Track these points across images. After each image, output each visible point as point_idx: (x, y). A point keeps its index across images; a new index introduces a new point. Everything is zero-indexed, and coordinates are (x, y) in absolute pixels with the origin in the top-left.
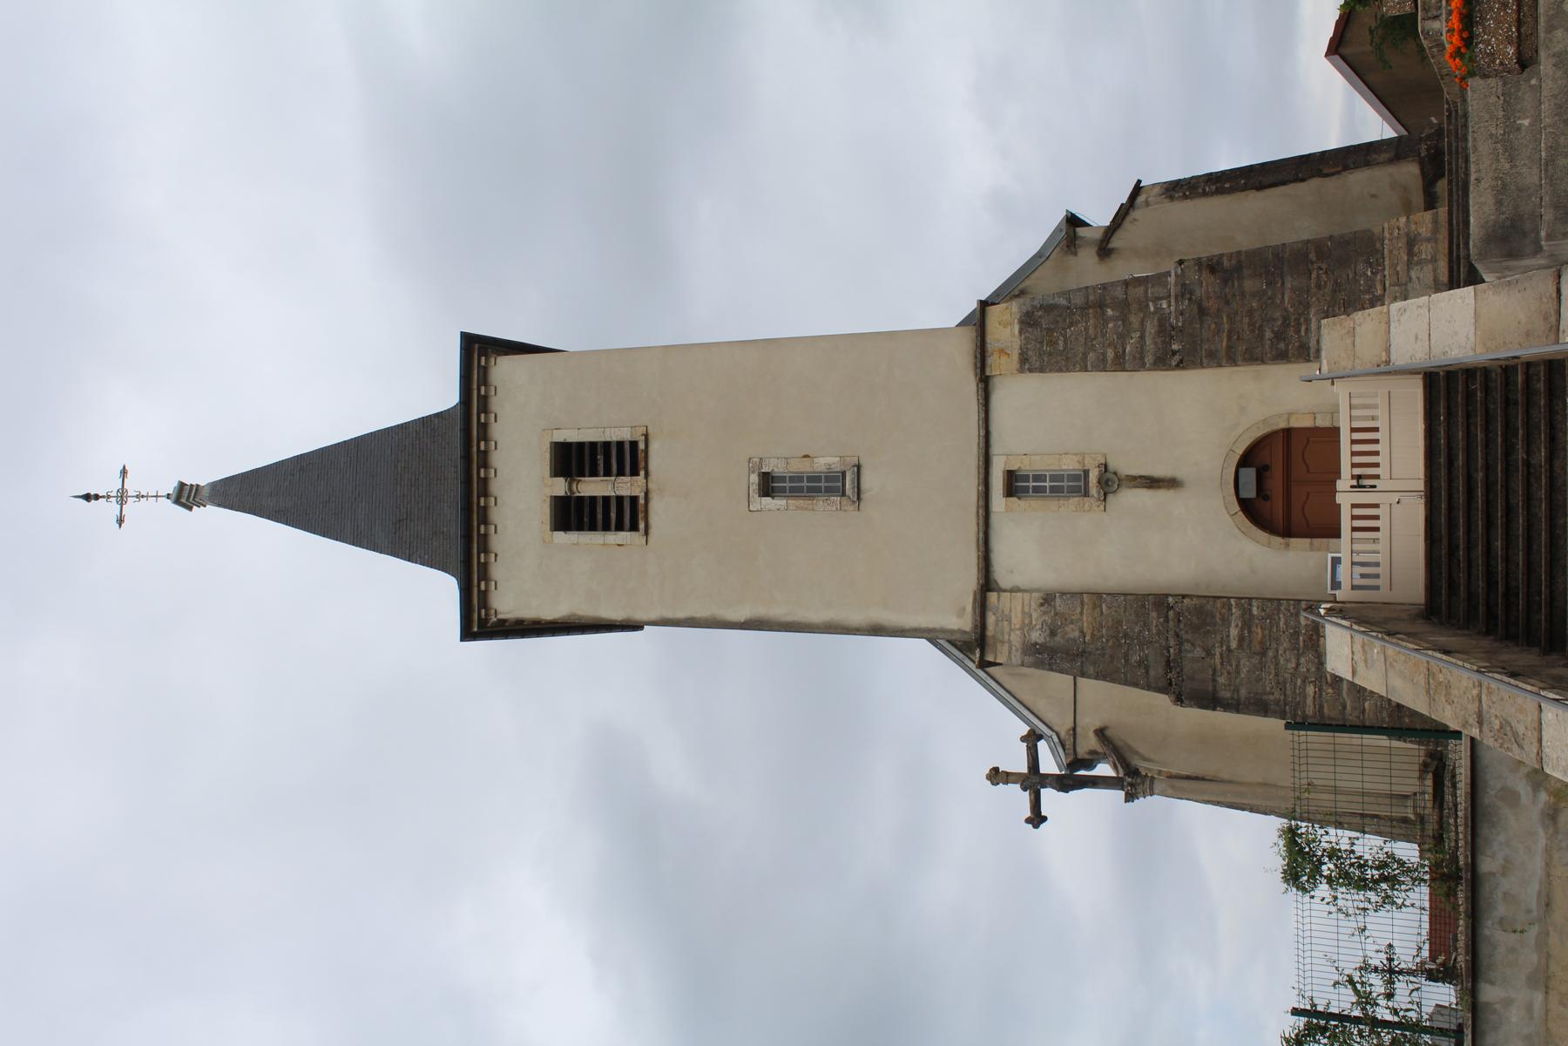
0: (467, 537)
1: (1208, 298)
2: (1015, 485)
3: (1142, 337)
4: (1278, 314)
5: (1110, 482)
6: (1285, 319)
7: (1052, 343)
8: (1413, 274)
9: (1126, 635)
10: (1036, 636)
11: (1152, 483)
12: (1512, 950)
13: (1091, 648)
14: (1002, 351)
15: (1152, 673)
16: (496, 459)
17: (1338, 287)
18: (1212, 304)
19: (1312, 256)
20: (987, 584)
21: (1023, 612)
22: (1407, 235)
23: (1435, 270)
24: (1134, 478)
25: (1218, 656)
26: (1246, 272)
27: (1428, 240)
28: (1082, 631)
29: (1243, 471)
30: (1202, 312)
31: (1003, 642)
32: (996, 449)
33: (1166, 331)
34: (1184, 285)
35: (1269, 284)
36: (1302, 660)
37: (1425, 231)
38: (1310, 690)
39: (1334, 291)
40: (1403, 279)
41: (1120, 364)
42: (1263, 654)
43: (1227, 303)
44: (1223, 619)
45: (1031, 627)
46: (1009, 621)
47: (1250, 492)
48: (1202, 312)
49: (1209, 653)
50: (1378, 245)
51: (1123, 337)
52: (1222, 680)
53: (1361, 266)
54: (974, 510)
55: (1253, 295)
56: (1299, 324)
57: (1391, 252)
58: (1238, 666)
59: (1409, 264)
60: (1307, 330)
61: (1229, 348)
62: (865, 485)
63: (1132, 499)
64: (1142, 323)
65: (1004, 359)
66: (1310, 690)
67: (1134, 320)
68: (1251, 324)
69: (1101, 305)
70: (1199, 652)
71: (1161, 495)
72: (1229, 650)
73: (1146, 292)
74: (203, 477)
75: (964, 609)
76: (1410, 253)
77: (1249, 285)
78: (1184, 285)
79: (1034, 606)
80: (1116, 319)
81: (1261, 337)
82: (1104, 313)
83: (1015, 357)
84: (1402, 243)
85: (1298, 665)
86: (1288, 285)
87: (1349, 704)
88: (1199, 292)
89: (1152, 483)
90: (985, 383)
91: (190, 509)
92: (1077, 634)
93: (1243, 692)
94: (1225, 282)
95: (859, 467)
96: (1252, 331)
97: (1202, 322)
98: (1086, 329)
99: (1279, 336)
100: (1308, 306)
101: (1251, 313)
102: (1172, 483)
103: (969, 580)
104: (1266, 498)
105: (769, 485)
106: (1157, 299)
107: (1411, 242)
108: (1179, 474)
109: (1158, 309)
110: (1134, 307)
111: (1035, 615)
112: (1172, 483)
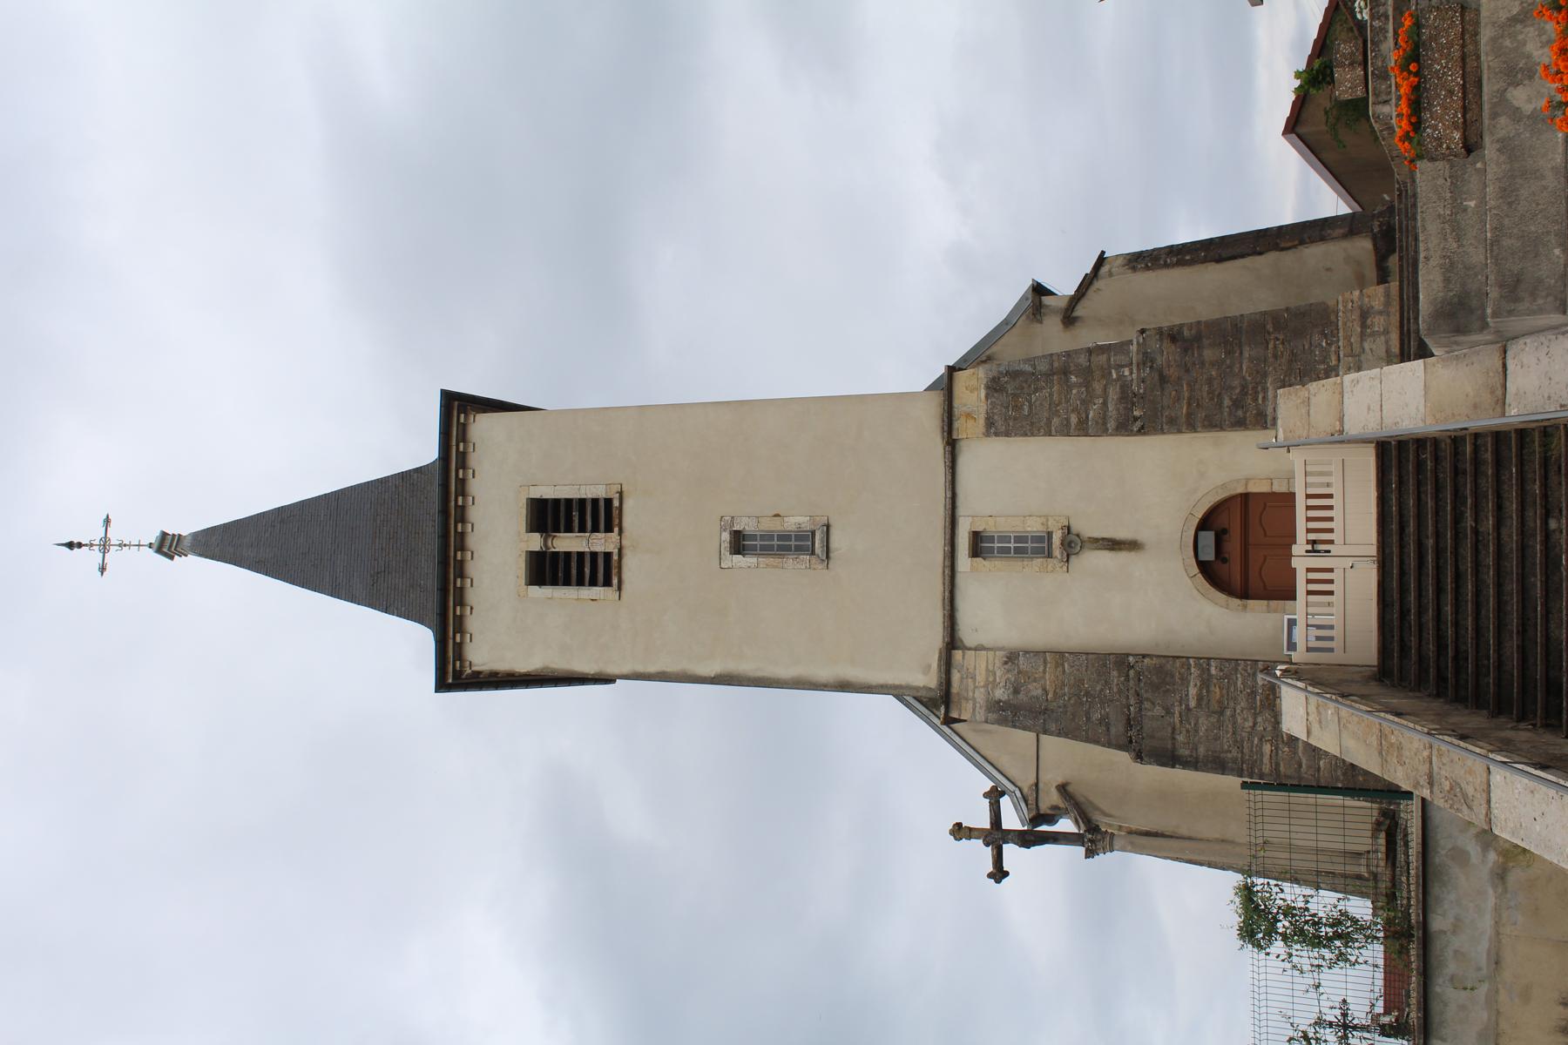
0: (444, 590)
2: (980, 545)
3: (1105, 403)
4: (1236, 383)
5: (1073, 544)
7: (1018, 408)
8: (1366, 345)
10: (1000, 694)
11: (1114, 545)
12: (1462, 1007)
14: (969, 416)
15: (1113, 730)
16: (474, 514)
17: (1293, 357)
18: (1172, 372)
19: (1270, 327)
20: (952, 643)
22: (1361, 308)
23: (1387, 342)
24: (1096, 540)
26: (1206, 342)
27: (1381, 313)
28: (1044, 689)
29: (1202, 534)
30: (1163, 379)
34: (1145, 353)
35: (1228, 353)
36: (1259, 719)
37: (1377, 304)
38: (1267, 748)
39: (1290, 361)
41: (1083, 430)
42: (1221, 713)
43: (1187, 371)
44: (1182, 679)
45: (995, 684)
46: (974, 678)
47: (1208, 554)
48: (1163, 379)
49: (1168, 711)
50: (1333, 317)
51: (1086, 403)
52: (1181, 738)
53: (1316, 337)
55: (1213, 364)
56: (1257, 393)
57: (1345, 324)
59: (1363, 336)
61: (1189, 415)
62: (833, 545)
63: (1094, 561)
65: (970, 422)
66: (1267, 748)
67: (1098, 387)
69: (1065, 372)
70: (1158, 711)
71: (1123, 557)
72: (1188, 709)
74: (186, 526)
76: (1364, 326)
77: (1208, 354)
78: (1145, 353)
79: (998, 664)
80: (1080, 385)
81: (1220, 405)
82: (1067, 380)
83: (982, 421)
84: (1356, 316)
85: (1255, 724)
86: (1246, 355)
87: (1304, 762)
89: (1114, 545)
91: (172, 558)
92: (1040, 692)
93: (1202, 750)
94: (1186, 350)
95: (828, 526)
98: (1051, 395)
99: (1237, 404)
100: (1265, 375)
101: (1210, 381)
102: (1132, 545)
103: (937, 638)
104: (1225, 561)
105: (739, 543)
106: (1119, 367)
107: (1365, 315)
109: (1121, 377)
110: (1097, 374)
111: (999, 674)
112: (1132, 545)
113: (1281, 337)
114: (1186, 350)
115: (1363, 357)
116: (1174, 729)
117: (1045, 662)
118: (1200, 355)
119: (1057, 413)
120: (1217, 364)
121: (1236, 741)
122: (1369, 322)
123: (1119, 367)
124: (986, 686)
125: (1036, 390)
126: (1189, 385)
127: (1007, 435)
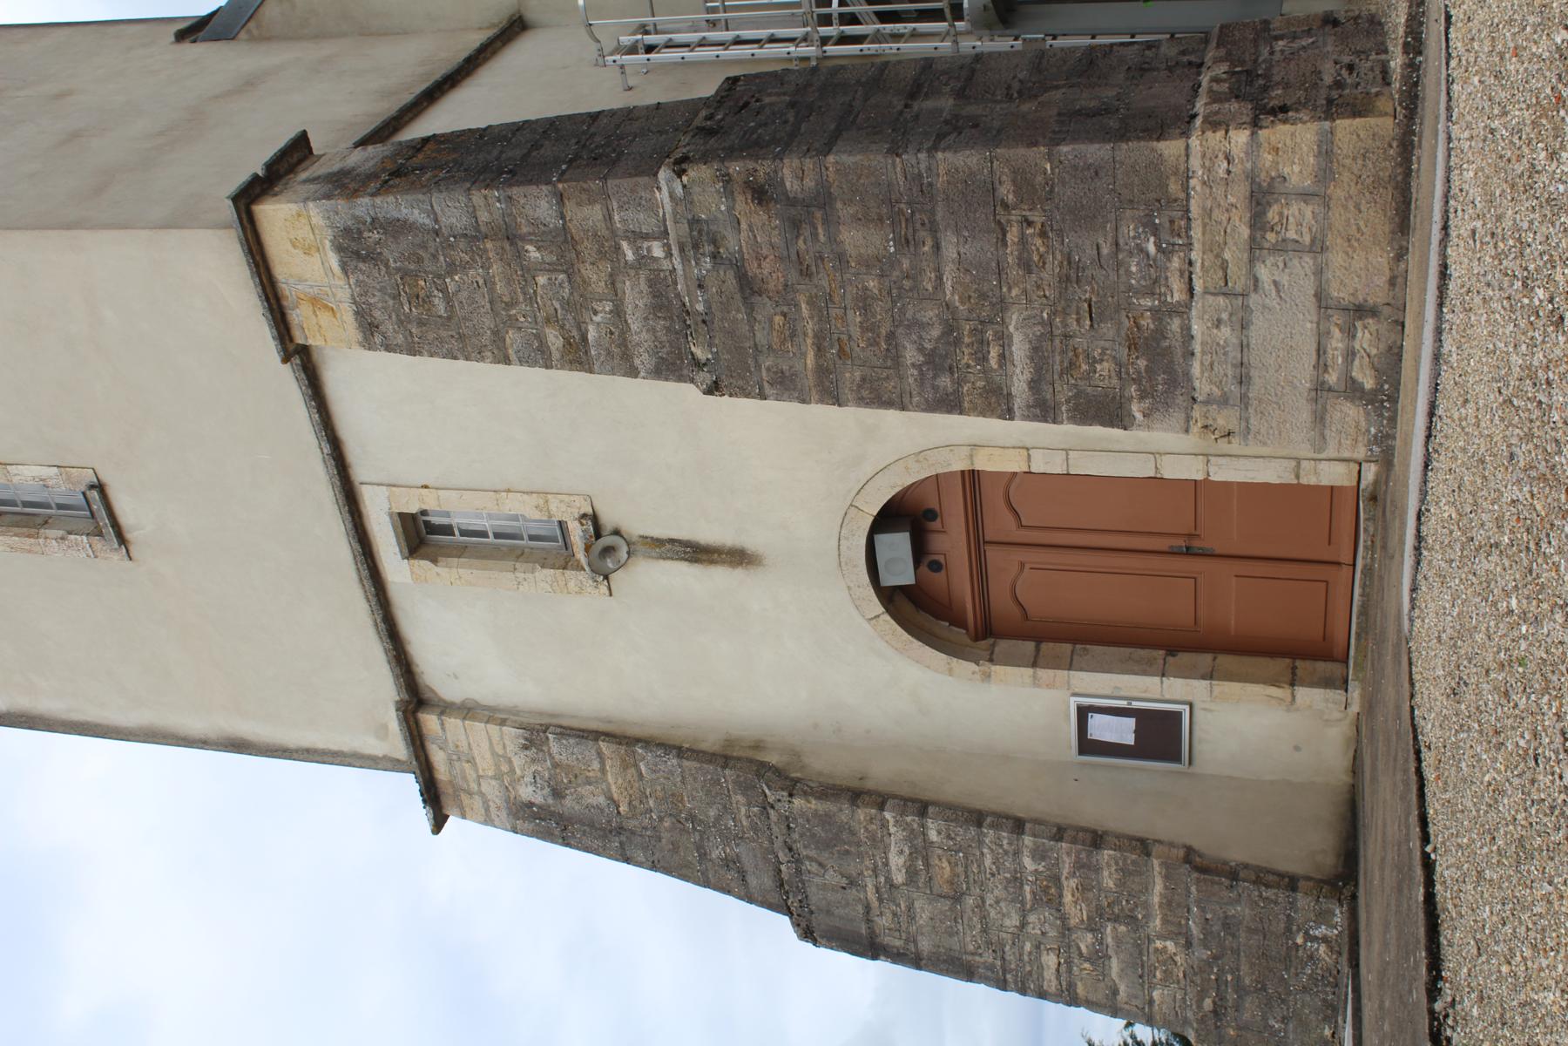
1: (760, 258)
3: (618, 313)
4: (930, 314)
6: (950, 328)
8: (1264, 273)
9: (692, 818)
13: (632, 824)
17: (1071, 275)
18: (769, 271)
19: (1006, 191)
21: (494, 753)
22: (1251, 177)
23: (1319, 272)
24: (658, 542)
25: (870, 888)
26: (844, 211)
27: (1305, 196)
28: (610, 798)
29: (882, 540)
31: (470, 794)
32: (360, 472)
33: (662, 300)
34: (694, 222)
35: (905, 243)
36: (1032, 918)
37: (1298, 172)
38: (1050, 960)
39: (1065, 280)
40: (1238, 281)
41: (577, 356)
42: (957, 898)
43: (806, 273)
44: (873, 838)
46: (471, 761)
48: (749, 287)
50: (1174, 187)
51: (579, 304)
53: (1129, 230)
54: (353, 575)
55: (867, 264)
56: (983, 343)
57: (1208, 213)
58: (910, 908)
59: (1255, 248)
60: (1002, 356)
63: (652, 578)
64: (612, 283)
65: (324, 318)
66: (1050, 960)
67: (595, 276)
68: (869, 327)
70: (832, 878)
71: (719, 577)
72: (892, 886)
73: (609, 217)
75: (385, 727)
76: (1258, 222)
77: (853, 239)
78: (694, 222)
79: (511, 748)
80: (551, 269)
81: (897, 361)
82: (520, 255)
84: (1238, 195)
85: (1023, 925)
86: (950, 251)
87: (1122, 988)
88: (732, 243)
90: (302, 359)
92: (601, 800)
94: (795, 225)
95: (100, 487)
96: (874, 343)
97: (751, 309)
99: (935, 362)
100: (1002, 305)
101: (864, 302)
102: (738, 557)
103: (385, 689)
104: (936, 567)
107: (1261, 196)
108: (750, 540)
109: (644, 260)
110: (588, 248)
111: (518, 762)
112: (738, 557)
113: (1037, 217)
114: (795, 225)
115: (1254, 299)
116: (868, 908)
117: (600, 754)
118: (833, 239)
119: (512, 322)
120: (880, 264)
121: (989, 943)
122: (1272, 215)
123: (637, 237)
124: (498, 777)
125: (452, 269)
126: (811, 303)
127: (413, 351)
